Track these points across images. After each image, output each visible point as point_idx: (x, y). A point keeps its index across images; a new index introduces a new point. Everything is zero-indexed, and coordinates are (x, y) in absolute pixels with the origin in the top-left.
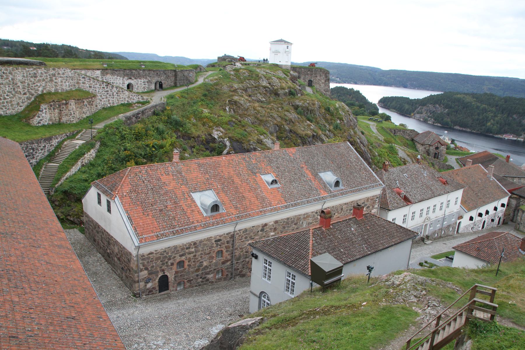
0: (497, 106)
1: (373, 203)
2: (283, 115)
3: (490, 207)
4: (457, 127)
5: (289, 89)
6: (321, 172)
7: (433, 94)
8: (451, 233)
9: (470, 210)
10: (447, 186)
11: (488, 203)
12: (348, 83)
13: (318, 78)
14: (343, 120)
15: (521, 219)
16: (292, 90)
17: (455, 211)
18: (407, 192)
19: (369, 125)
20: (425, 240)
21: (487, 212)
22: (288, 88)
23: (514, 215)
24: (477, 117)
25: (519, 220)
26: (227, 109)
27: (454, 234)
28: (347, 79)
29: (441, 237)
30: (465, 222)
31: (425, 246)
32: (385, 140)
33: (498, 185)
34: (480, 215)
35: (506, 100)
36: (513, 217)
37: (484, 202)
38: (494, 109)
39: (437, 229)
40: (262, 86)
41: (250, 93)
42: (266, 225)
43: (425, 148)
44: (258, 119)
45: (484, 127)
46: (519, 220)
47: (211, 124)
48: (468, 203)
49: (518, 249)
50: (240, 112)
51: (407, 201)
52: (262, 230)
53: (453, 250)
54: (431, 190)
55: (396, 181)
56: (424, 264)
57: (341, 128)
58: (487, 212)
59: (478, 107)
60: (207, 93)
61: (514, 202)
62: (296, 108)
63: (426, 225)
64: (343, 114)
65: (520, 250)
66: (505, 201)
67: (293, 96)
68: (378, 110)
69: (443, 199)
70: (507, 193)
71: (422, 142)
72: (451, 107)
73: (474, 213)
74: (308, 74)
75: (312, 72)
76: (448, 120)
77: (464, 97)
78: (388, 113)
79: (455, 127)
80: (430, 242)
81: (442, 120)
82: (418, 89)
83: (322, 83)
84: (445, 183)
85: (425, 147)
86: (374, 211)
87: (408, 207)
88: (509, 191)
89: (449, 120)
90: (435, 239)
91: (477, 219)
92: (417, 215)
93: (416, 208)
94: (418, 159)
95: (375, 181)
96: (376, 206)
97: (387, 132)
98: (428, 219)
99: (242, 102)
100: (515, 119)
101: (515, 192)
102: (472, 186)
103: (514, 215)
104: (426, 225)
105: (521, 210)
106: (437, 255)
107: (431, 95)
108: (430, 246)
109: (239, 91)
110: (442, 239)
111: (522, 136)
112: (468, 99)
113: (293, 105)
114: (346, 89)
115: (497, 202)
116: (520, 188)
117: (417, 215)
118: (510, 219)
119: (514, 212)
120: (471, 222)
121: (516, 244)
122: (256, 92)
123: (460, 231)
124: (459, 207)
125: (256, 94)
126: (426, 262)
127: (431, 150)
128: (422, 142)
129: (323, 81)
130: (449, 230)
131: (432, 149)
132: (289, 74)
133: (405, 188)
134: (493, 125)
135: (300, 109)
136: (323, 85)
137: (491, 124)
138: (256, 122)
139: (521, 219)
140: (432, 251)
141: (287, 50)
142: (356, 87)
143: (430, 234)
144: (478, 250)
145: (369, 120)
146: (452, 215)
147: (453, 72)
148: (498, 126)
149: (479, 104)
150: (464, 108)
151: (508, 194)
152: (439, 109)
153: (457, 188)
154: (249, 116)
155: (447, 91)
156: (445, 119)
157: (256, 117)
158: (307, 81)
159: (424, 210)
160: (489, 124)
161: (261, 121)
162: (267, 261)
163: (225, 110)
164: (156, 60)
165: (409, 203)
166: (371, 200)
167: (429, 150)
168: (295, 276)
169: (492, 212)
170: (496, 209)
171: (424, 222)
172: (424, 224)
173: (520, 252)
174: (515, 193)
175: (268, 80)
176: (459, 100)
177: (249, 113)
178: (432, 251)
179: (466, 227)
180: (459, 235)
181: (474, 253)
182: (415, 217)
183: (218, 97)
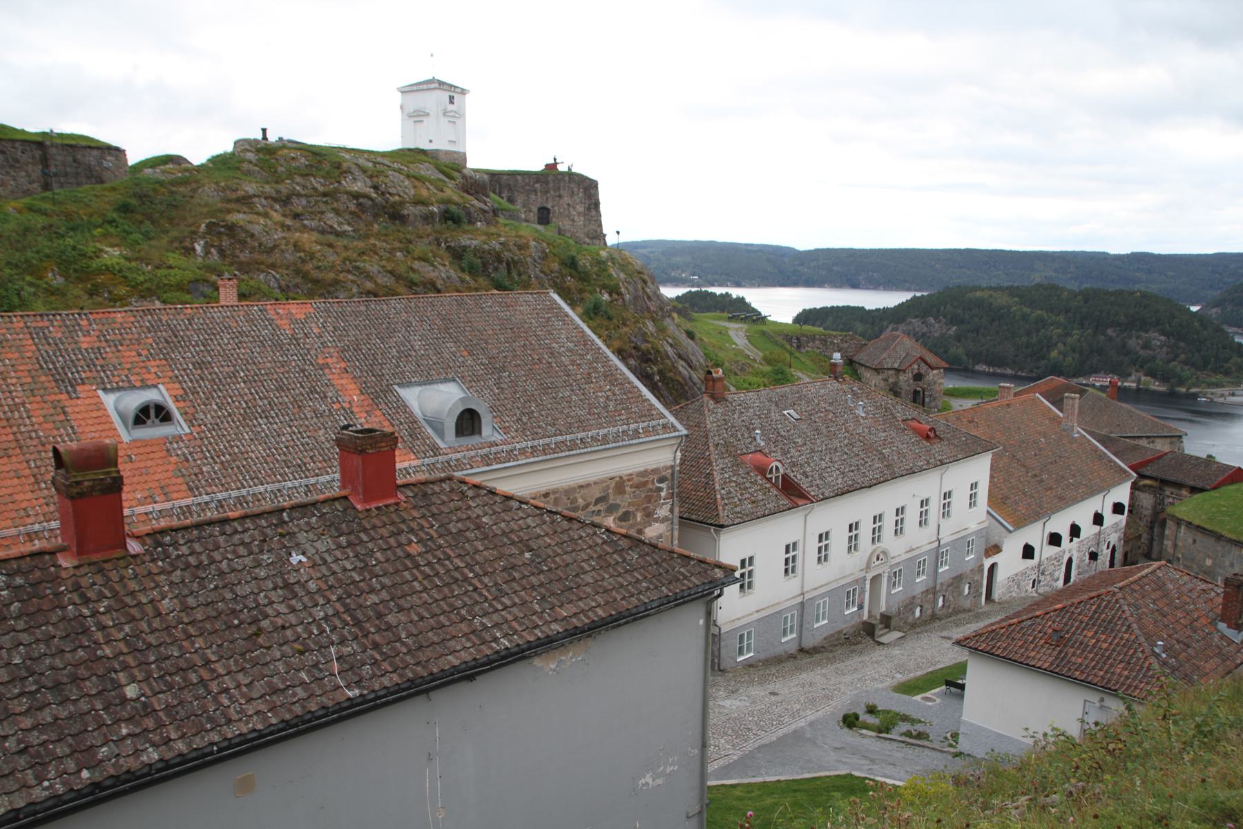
0: (1067, 311)
1: (648, 499)
2: (402, 269)
3: (1082, 513)
4: (984, 368)
5: (443, 207)
6: (409, 384)
8: (967, 604)
9: (1020, 522)
10: (937, 445)
11: (1075, 501)
13: (566, 199)
14: (619, 294)
15: (1175, 546)
16: (453, 208)
17: (974, 527)
18: (794, 464)
19: (727, 329)
20: (878, 633)
21: (1075, 531)
22: (442, 202)
23: (1151, 540)
24: (1024, 339)
25: (1170, 550)
26: (198, 248)
27: (976, 604)
28: (717, 277)
29: (934, 617)
30: (1009, 563)
31: (878, 653)
32: (765, 359)
33: (1096, 450)
34: (1055, 539)
36: (1150, 547)
37: (1061, 498)
38: (1061, 319)
39: (918, 590)
40: (348, 193)
41: (300, 210)
43: (886, 380)
44: (305, 276)
45: (1043, 362)
46: (1170, 550)
47: (122, 290)
48: (1015, 500)
49: (1213, 623)
50: (244, 256)
51: (793, 494)
53: (961, 655)
54: (883, 457)
55: (754, 429)
56: (865, 718)
57: (611, 312)
58: (1075, 531)
59: (1025, 317)
60: (134, 202)
61: (1147, 500)
62: (457, 254)
63: (876, 579)
64: (622, 276)
65: (1222, 626)
66: (1122, 494)
67: (453, 226)
69: (927, 486)
70: (1125, 472)
71: (875, 364)
72: (962, 322)
73: (1035, 534)
74: (535, 191)
75: (547, 183)
76: (958, 350)
77: (991, 296)
79: (977, 368)
80: (896, 635)
81: (946, 352)
82: (885, 289)
83: (579, 214)
84: (929, 436)
85: (884, 376)
86: (653, 532)
88: (1131, 467)
89: (961, 351)
90: (914, 626)
91: (1046, 552)
92: (838, 543)
93: (832, 517)
94: (835, 365)
95: (649, 413)
96: (663, 512)
97: (776, 343)
98: (881, 556)
99: (256, 229)
100: (1111, 339)
101: (1148, 471)
102: (1020, 455)
103: (1151, 540)
104: (876, 579)
105: (1173, 517)
106: (917, 679)
108: (896, 651)
109: (259, 204)
110: (937, 624)
111: (1133, 378)
112: (1002, 300)
113: (448, 248)
114: (713, 295)
115: (1099, 497)
116: (1159, 458)
117: (838, 543)
118: (1144, 539)
119: (1151, 528)
120: (1029, 562)
121: (1202, 605)
122: (323, 207)
123: (996, 595)
124: (984, 516)
125: (322, 213)
126: (871, 710)
127: (902, 383)
128: (876, 362)
129: (580, 208)
130: (961, 593)
131: (905, 379)
132: (456, 174)
133: (784, 453)
134: (1065, 356)
135: (469, 257)
136: (580, 221)
137: (1060, 353)
138: (297, 286)
139: (1175, 546)
140: (900, 668)
141: (451, 107)
142: (735, 292)
143: (894, 610)
144: (1059, 640)
145: (730, 319)
146: (963, 543)
147: (963, 247)
148: (1077, 356)
149: (1026, 310)
150: (993, 321)
151: (1128, 476)
152: (937, 328)
153: (971, 449)
154: (273, 266)
156: (952, 350)
157: (298, 272)
158: (535, 210)
159: (861, 526)
160: (1054, 354)
161: (316, 282)
163: (190, 251)
165: (800, 502)
166: (637, 486)
167: (896, 384)
169: (1088, 530)
170: (1098, 519)
171: (868, 567)
172: (869, 576)
173: (1223, 637)
174: (1148, 474)
175: (371, 177)
176: (979, 304)
177: (276, 257)
178: (900, 668)
179: (1015, 580)
180: (997, 607)
181: (1045, 657)
182: (832, 552)
183: (174, 214)
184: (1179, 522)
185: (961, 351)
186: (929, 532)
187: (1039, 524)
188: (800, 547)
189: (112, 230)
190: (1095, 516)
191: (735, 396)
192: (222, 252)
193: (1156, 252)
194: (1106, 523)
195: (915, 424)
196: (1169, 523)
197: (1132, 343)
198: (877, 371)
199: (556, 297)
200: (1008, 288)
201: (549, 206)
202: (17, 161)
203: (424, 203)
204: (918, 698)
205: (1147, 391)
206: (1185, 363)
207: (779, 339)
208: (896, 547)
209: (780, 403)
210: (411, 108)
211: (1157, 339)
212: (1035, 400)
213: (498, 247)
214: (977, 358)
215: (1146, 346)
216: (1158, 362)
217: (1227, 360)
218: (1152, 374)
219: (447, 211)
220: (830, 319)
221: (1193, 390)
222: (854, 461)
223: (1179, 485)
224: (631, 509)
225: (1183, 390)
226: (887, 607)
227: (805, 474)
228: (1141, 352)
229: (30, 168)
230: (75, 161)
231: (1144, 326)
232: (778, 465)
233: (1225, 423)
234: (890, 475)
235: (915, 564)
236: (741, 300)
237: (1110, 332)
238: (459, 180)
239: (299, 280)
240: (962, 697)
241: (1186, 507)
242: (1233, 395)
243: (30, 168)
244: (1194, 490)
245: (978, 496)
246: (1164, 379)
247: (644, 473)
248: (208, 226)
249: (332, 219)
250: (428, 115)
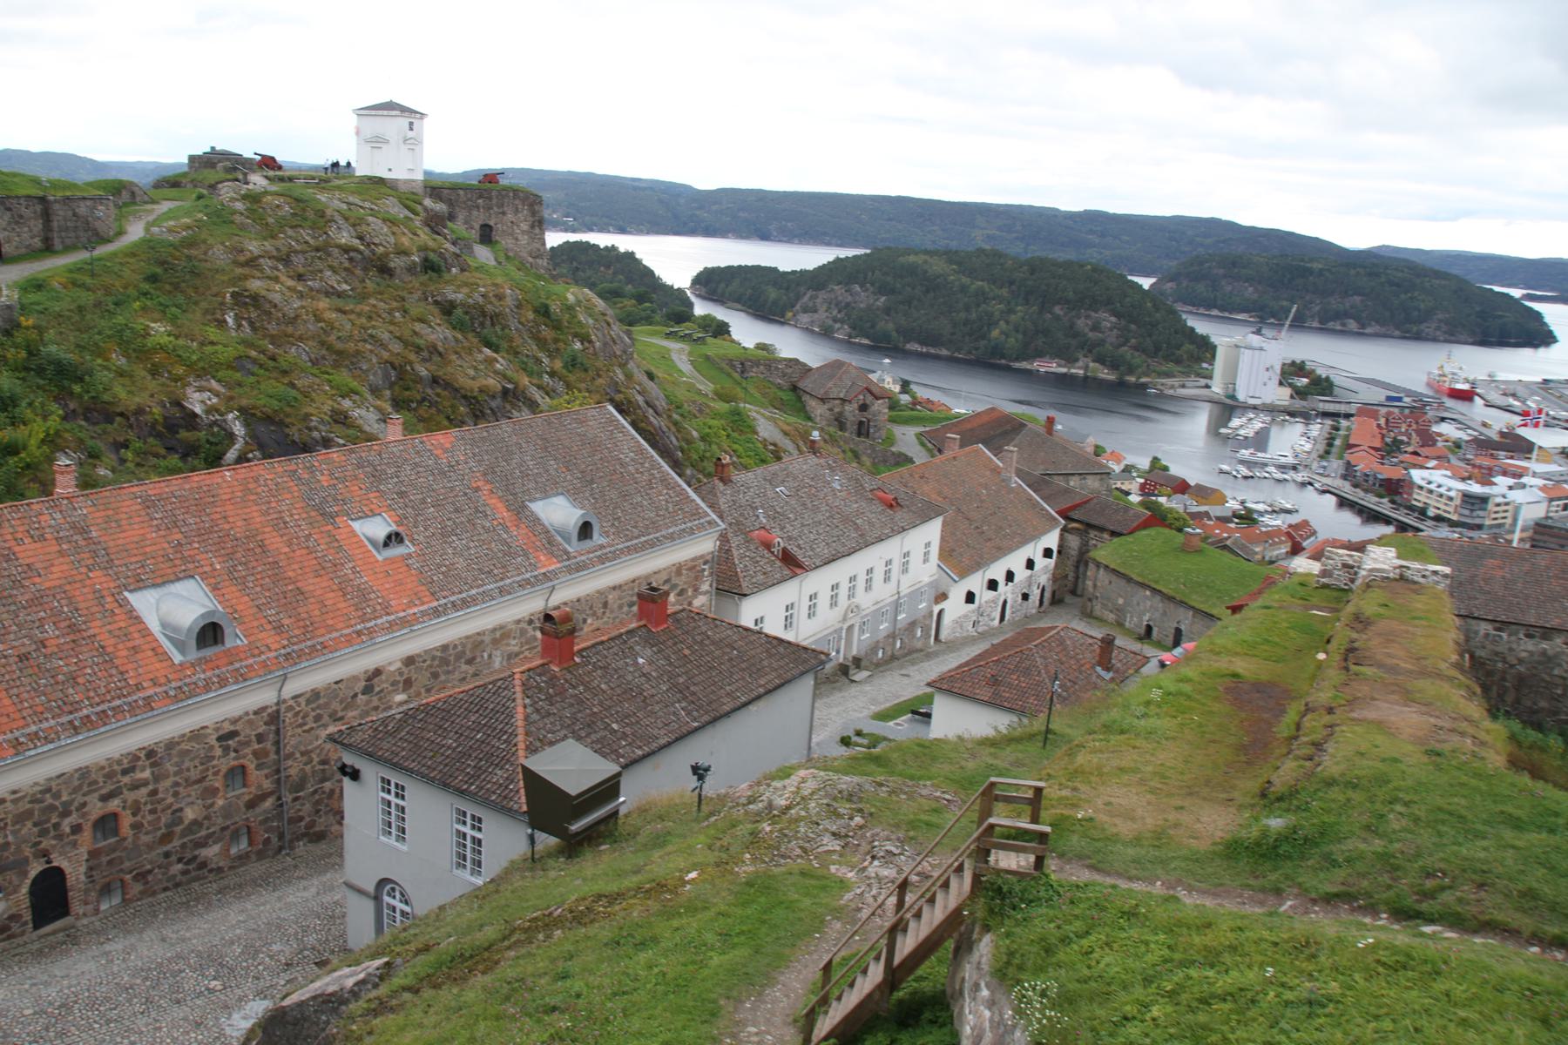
0: (1011, 283)
1: (696, 578)
2: (407, 334)
3: (1016, 561)
6: (535, 500)
8: (919, 645)
9: (964, 573)
10: (900, 511)
11: (1011, 550)
13: (510, 217)
14: (590, 342)
15: (1095, 586)
16: (432, 256)
17: (926, 580)
18: (790, 538)
21: (1010, 576)
23: (1077, 578)
24: (963, 315)
26: (230, 321)
29: (893, 658)
31: (854, 689)
32: (716, 393)
33: (1030, 499)
34: (993, 585)
35: (1035, 266)
36: (1076, 584)
37: (999, 548)
38: (1004, 292)
40: (339, 246)
42: (378, 672)
45: (983, 343)
47: (180, 370)
48: (960, 555)
49: (1093, 667)
50: (273, 328)
51: (792, 564)
52: (368, 690)
53: (929, 690)
54: (857, 528)
56: (855, 739)
58: (1010, 576)
59: (963, 289)
60: (159, 270)
61: (1074, 542)
62: (447, 309)
63: (851, 628)
64: (591, 321)
65: (1099, 669)
67: (434, 275)
68: (691, 305)
69: (891, 549)
71: (821, 393)
72: (893, 291)
73: (976, 582)
75: (490, 199)
77: (926, 262)
79: (908, 346)
80: (865, 674)
81: (873, 327)
82: (800, 243)
83: (523, 232)
86: (699, 602)
89: (891, 326)
90: (878, 665)
92: (823, 601)
93: (818, 582)
94: (813, 442)
95: (696, 513)
96: (705, 587)
97: (721, 370)
99: (276, 298)
100: (1058, 318)
101: (1075, 515)
102: (964, 508)
103: (1077, 578)
104: (851, 628)
107: (838, 260)
108: (867, 688)
110: (896, 663)
111: (1080, 363)
112: (938, 266)
113: (436, 303)
114: (595, 247)
115: (1032, 545)
117: (823, 601)
119: (1077, 567)
121: (1088, 655)
123: (943, 636)
124: (935, 569)
126: (859, 733)
127: (847, 414)
129: (524, 226)
131: (850, 410)
132: (419, 208)
134: (1007, 336)
135: (459, 312)
136: (524, 239)
137: (1002, 333)
138: (324, 358)
139: (1095, 586)
140: (874, 701)
141: (411, 134)
144: (994, 682)
145: (669, 335)
146: (916, 594)
147: (893, 194)
148: (1020, 336)
150: (928, 291)
152: (863, 298)
153: (925, 518)
154: (301, 338)
157: (322, 343)
158: (477, 227)
161: (340, 353)
163: (222, 323)
165: (798, 571)
169: (1021, 574)
170: (1030, 564)
171: (844, 619)
173: (1099, 676)
175: (354, 225)
176: (912, 270)
177: (301, 330)
179: (958, 623)
180: (943, 647)
181: (985, 693)
184: (1098, 565)
185: (891, 326)
187: (980, 573)
189: (149, 303)
190: (1030, 561)
191: (739, 477)
192: (251, 324)
193: (1111, 211)
194: (1037, 567)
195: (881, 494)
196: (1091, 566)
197: (1081, 323)
198: (823, 400)
199: (611, 408)
200: (946, 253)
202: (21, 217)
203: (405, 253)
204: (891, 724)
205: (1095, 379)
206: (1136, 348)
207: (724, 365)
208: (865, 600)
209: (772, 481)
210: (368, 133)
211: (1107, 320)
212: (978, 451)
213: (481, 300)
214: (909, 335)
215: (1096, 327)
216: (1108, 346)
217: (1179, 347)
218: (1100, 360)
219: (426, 260)
220: (736, 282)
221: (1143, 380)
222: (835, 532)
223: (1101, 529)
225: (1133, 379)
227: (799, 546)
228: (1091, 334)
229: (32, 223)
230: (75, 214)
231: (1095, 304)
232: (779, 541)
234: (864, 543)
235: (878, 614)
237: (1057, 310)
238: (423, 214)
239: (324, 352)
240: (929, 723)
241: (1106, 551)
242: (1183, 386)
243: (32, 223)
244: (1114, 534)
246: (1114, 366)
247: (693, 560)
248: (233, 295)
249: (332, 279)
250: (387, 142)
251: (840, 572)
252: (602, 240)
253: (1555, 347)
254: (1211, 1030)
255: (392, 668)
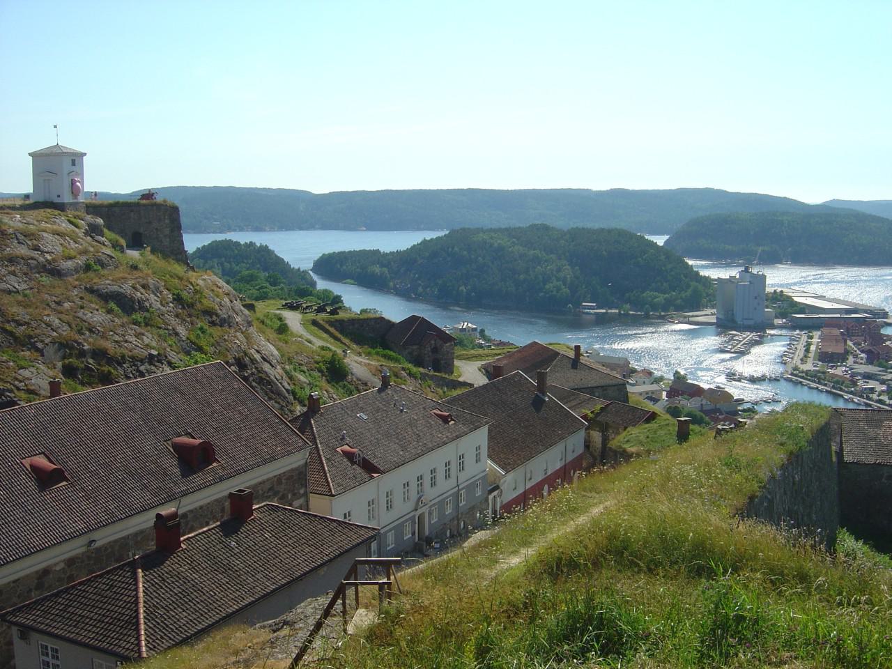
7: (428, 238)
12: (241, 230)
35: (575, 234)
42: (46, 572)
52: (39, 586)
68: (314, 284)
69: (448, 453)
78: (336, 288)
87: (372, 484)
93: (390, 482)
107: (425, 242)
114: (238, 244)
129: (167, 231)
142: (259, 239)
155: (457, 227)
162: (47, 647)
164: (824, 266)
168: (57, 651)
186: (452, 482)
188: (376, 502)
193: (631, 188)
201: (141, 231)
208: (431, 494)
224: (286, 492)
226: (430, 533)
233: (835, 208)
235: (442, 505)
236: (265, 250)
245: (481, 454)
251: (409, 472)
252: (243, 238)
253: (44, 142)
254: (37, 394)
255: (58, 568)
